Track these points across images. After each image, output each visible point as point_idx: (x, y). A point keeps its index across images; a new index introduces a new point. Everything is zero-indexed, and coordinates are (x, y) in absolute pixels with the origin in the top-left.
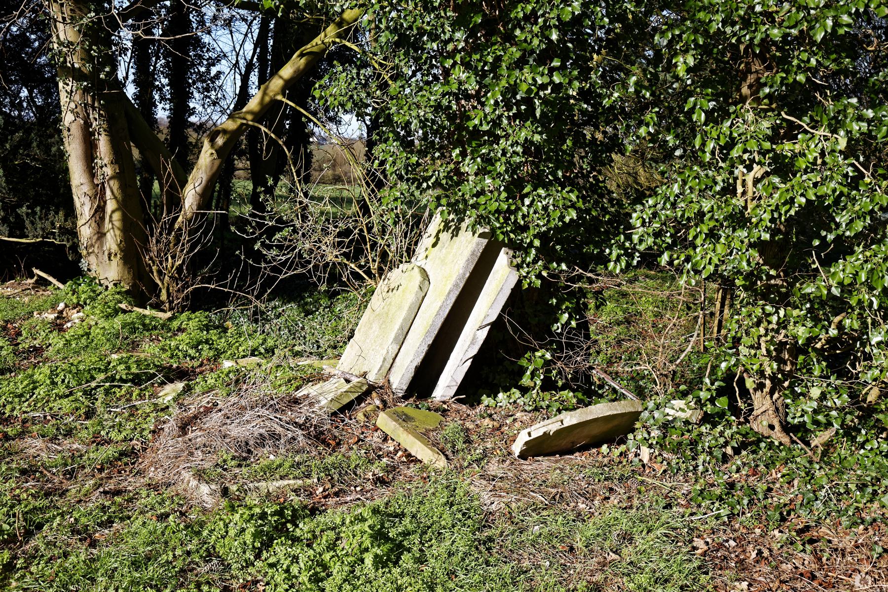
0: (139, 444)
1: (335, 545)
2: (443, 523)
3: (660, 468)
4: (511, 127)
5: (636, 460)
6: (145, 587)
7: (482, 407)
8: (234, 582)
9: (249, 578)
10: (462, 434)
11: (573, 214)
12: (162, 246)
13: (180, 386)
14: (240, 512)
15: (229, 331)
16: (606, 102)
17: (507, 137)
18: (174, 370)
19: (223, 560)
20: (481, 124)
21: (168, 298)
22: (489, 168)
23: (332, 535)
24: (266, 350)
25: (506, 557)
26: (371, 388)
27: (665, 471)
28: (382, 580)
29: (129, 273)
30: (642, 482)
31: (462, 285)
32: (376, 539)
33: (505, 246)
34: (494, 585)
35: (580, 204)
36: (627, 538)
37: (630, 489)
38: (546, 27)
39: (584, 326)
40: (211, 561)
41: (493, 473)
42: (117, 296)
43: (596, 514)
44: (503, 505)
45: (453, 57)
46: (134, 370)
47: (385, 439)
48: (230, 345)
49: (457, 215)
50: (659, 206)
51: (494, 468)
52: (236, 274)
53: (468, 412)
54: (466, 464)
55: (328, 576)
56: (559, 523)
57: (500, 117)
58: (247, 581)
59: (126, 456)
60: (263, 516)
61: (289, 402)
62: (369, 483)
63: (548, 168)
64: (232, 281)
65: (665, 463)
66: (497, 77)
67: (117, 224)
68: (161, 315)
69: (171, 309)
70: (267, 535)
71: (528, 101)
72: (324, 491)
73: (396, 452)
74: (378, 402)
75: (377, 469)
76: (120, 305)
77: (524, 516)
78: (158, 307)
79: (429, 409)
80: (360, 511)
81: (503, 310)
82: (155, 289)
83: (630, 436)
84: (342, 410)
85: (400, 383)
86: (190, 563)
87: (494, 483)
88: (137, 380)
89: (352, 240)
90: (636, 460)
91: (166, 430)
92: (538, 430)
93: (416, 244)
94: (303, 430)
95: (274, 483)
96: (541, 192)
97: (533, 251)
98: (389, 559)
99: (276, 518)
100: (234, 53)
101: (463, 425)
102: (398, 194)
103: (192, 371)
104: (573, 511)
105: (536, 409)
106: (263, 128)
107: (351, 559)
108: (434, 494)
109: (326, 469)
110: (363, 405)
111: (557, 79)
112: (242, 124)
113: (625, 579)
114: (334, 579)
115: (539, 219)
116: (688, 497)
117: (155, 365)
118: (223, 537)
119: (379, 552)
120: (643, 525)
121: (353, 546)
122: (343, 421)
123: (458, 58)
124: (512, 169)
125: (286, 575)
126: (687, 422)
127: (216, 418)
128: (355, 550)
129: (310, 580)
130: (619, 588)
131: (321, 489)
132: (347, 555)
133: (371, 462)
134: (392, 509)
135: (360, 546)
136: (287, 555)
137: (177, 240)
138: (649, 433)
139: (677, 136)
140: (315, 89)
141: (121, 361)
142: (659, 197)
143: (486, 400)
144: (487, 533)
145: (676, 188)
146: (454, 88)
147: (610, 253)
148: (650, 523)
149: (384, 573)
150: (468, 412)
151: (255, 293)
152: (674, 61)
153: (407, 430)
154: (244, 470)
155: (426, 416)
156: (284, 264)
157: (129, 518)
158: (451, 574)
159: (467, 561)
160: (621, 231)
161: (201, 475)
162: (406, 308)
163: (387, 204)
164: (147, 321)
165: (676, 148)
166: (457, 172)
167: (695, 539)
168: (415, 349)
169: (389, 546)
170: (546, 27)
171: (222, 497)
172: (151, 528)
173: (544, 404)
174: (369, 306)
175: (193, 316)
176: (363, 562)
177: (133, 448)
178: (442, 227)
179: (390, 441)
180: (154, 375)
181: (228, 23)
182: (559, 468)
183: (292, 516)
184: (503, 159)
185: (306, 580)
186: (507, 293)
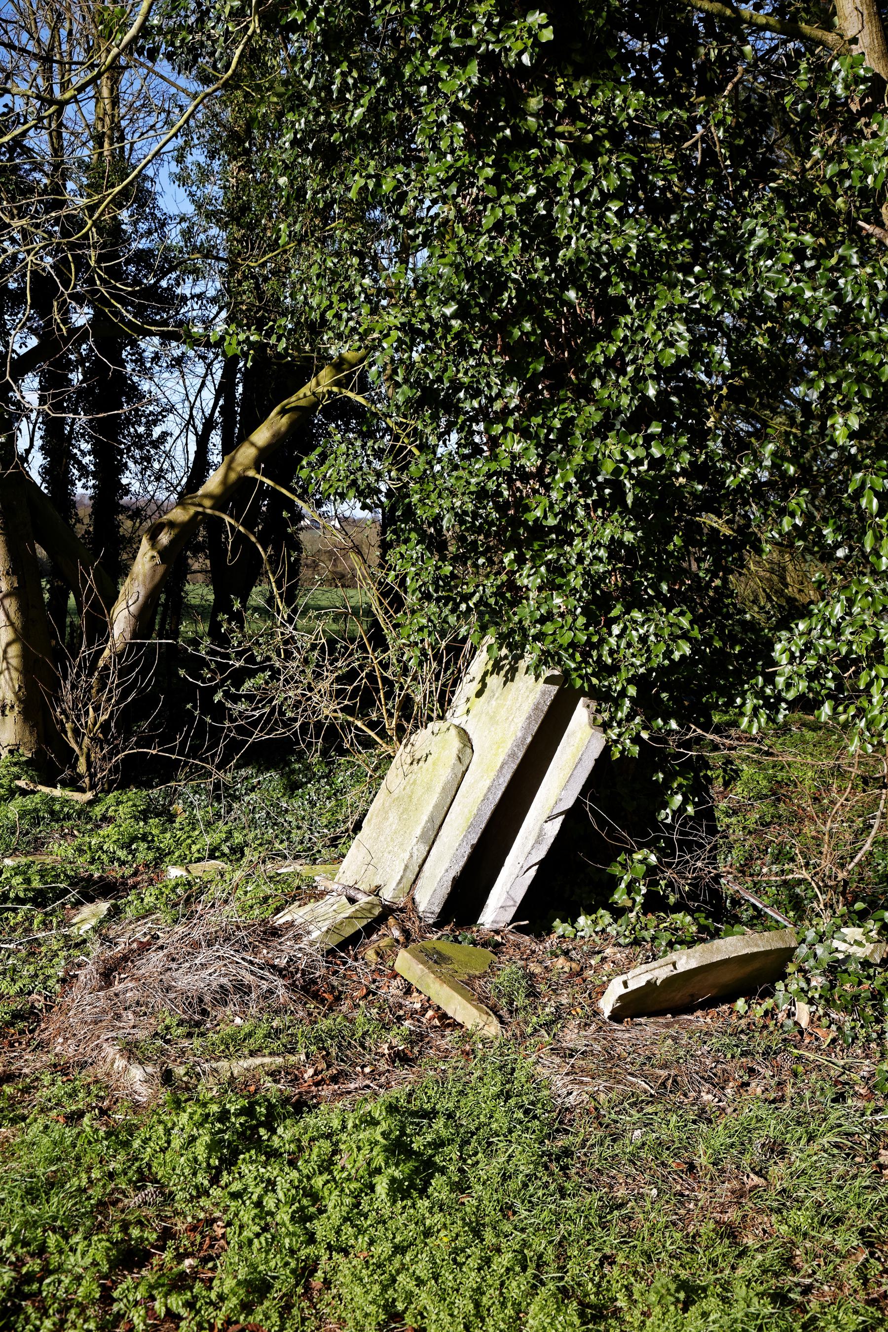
0: (42, 999)
1: (331, 1163)
2: (494, 1126)
3: (826, 1036)
4: (590, 520)
5: (790, 1022)
6: (45, 1231)
7: (554, 937)
8: (178, 1220)
9: (202, 1215)
10: (524, 983)
11: (686, 649)
12: (79, 693)
13: (103, 907)
14: (189, 1110)
15: (178, 820)
16: (731, 482)
17: (584, 535)
18: (96, 883)
19: (163, 1186)
20: (545, 517)
21: (88, 769)
22: (559, 581)
23: (325, 1146)
24: (231, 849)
25: (590, 1181)
26: (388, 911)
27: (834, 1041)
28: (402, 1220)
29: (31, 733)
30: (799, 1058)
31: (520, 755)
32: (394, 1154)
33: (585, 695)
34: (571, 1228)
35: (696, 633)
36: (777, 1149)
37: (780, 1068)
38: (638, 379)
39: (706, 815)
40: (144, 1187)
41: (571, 1045)
42: (14, 769)
43: (729, 1110)
44: (585, 1097)
45: (504, 422)
46: (36, 884)
47: (408, 990)
48: (179, 843)
49: (511, 651)
50: (815, 633)
51: (571, 1037)
52: (188, 732)
53: (534, 946)
54: (529, 1030)
55: (321, 1211)
56: (671, 1126)
57: (573, 505)
58: (199, 1220)
59: (23, 1018)
60: (223, 1116)
61: (265, 933)
62: (383, 1061)
63: (647, 579)
64: (183, 743)
65: (834, 1027)
66: (569, 450)
67: (14, 662)
68: (77, 796)
69: (93, 787)
70: (228, 1147)
71: (616, 485)
72: (316, 1073)
73: (424, 1010)
74: (397, 933)
75: (395, 1039)
76: (17, 782)
77: (618, 1113)
78: (73, 784)
79: (474, 943)
80: (369, 1108)
81: (583, 792)
82: (69, 758)
83: (780, 986)
84: (343, 945)
85: (430, 903)
86: (113, 1190)
87: (572, 1061)
88: (40, 899)
89: (357, 688)
90: (790, 1022)
91: (82, 978)
92: (638, 977)
93: (454, 685)
94: (284, 977)
95: (241, 1062)
96: (637, 615)
97: (627, 703)
98: (412, 1186)
99: (242, 1119)
100: (187, 404)
101: (524, 968)
102: (424, 621)
103: (122, 884)
104: (693, 1105)
105: (636, 942)
106: (227, 519)
107: (354, 1185)
108: (481, 1078)
109: (319, 1039)
110: (374, 937)
111: (656, 452)
112: (197, 514)
113: (774, 1218)
114: (329, 1218)
115: (634, 656)
116: (871, 1083)
117: (66, 875)
118: (163, 1150)
119: (397, 1174)
120: (800, 1130)
121: (357, 1165)
122: (345, 963)
123: (510, 423)
124: (593, 582)
125: (256, 1211)
126: (866, 964)
127: (156, 958)
128: (361, 1172)
129: (292, 1218)
130: (765, 1231)
131: (311, 1071)
132: (348, 1179)
133: (386, 1027)
134: (418, 1103)
135: (369, 1164)
136: (259, 1179)
137: (102, 684)
138: (808, 981)
139: (837, 529)
140: (302, 467)
141: (17, 871)
142: (814, 619)
143: (560, 927)
144: (563, 1141)
145: (838, 610)
146: (505, 465)
147: (743, 704)
148: (812, 1126)
149: (404, 1208)
150: (534, 946)
151: (217, 761)
152: (829, 423)
153: (440, 977)
154: (197, 1042)
155: (469, 955)
156: (255, 724)
157: (24, 1118)
158: (507, 1210)
159: (531, 1188)
160: (759, 669)
161: (131, 1050)
162: (438, 789)
163: (409, 636)
164: (57, 807)
165: (837, 545)
166: (511, 585)
167: (882, 1151)
168: (452, 851)
169: (411, 1164)
170: (638, 379)
171: (163, 1085)
172: (56, 1135)
173: (647, 935)
174: (383, 786)
175: (125, 798)
176: (373, 1191)
177: (33, 1007)
178: (490, 667)
179: (415, 994)
180: (65, 892)
181: (179, 362)
182: (671, 1036)
183: (266, 1116)
184: (580, 569)
185: (287, 1218)
186: (588, 766)
